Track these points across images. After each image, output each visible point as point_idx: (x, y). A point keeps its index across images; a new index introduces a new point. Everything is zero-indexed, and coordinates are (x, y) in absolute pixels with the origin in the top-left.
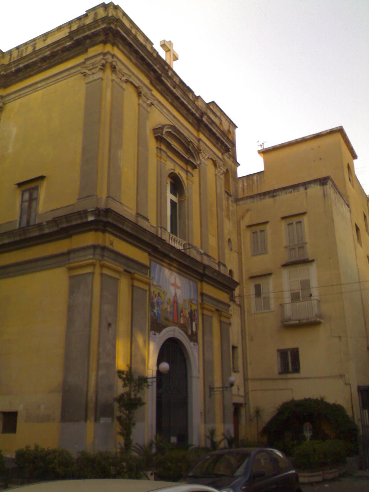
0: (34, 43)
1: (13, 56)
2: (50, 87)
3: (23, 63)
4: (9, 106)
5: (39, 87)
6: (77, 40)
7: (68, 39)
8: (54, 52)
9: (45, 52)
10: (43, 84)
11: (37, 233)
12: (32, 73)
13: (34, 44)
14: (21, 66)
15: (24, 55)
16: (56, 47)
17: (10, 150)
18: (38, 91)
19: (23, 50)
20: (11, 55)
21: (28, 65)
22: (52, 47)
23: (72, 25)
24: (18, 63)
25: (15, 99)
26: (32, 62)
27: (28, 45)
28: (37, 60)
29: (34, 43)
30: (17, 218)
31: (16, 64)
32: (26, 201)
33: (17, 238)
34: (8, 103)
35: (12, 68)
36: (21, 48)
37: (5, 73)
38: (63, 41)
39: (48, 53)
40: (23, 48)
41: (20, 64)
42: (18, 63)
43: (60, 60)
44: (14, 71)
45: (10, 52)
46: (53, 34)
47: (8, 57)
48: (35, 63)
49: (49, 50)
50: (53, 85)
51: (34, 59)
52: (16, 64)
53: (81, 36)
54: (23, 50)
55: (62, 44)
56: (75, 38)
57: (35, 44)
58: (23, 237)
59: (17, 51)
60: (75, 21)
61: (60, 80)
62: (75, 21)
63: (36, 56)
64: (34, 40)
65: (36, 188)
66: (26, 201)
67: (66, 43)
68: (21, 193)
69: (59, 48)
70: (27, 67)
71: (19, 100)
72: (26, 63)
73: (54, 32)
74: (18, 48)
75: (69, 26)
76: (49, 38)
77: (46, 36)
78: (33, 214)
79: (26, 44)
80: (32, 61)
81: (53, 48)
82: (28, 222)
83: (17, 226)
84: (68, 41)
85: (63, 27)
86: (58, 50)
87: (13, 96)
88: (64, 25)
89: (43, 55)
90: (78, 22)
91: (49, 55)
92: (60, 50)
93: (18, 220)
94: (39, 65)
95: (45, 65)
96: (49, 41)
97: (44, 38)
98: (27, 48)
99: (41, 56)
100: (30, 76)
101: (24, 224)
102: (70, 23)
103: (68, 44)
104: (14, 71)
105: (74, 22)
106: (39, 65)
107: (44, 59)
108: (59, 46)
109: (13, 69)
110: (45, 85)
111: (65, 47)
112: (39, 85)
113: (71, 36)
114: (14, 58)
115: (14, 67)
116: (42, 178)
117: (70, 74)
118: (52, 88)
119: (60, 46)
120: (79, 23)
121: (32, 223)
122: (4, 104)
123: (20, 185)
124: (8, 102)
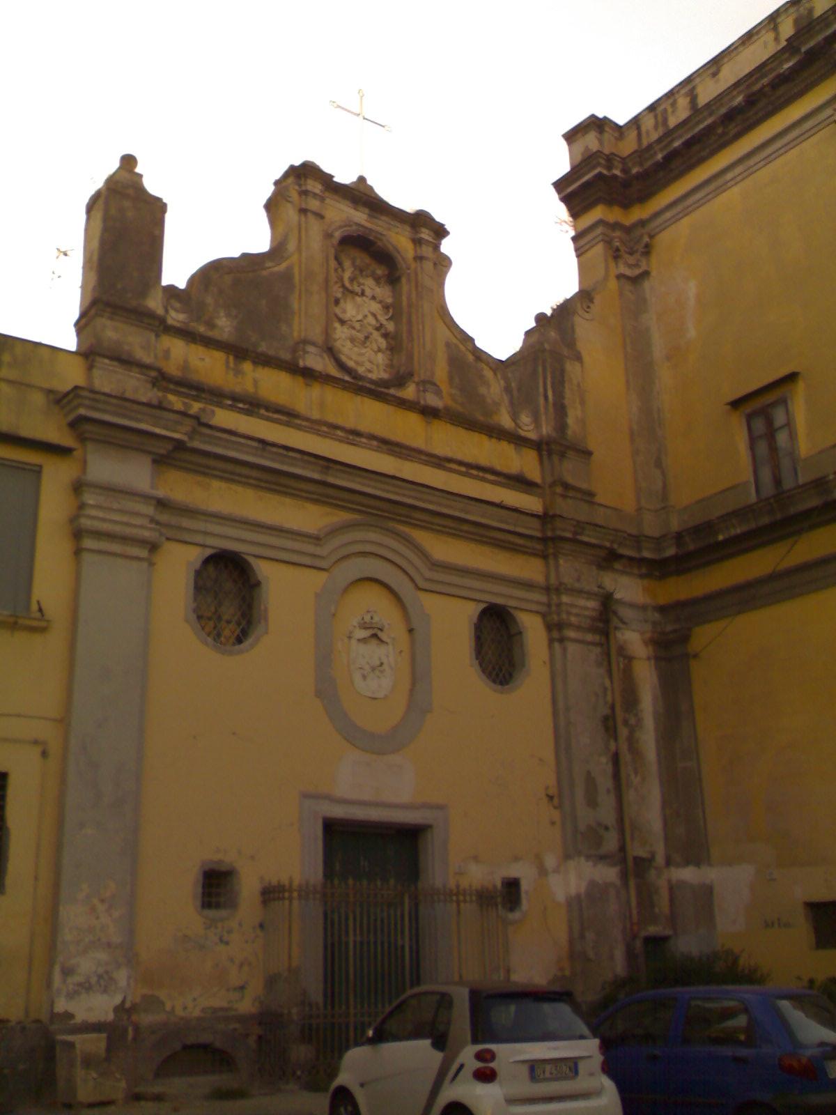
0: (689, 87)
1: (644, 129)
2: (758, 173)
3: (680, 136)
4: (664, 239)
5: (732, 179)
6: (807, 53)
7: (787, 55)
8: (754, 94)
9: (734, 98)
10: (738, 170)
11: (814, 502)
12: (703, 154)
13: (689, 91)
14: (677, 144)
15: (672, 122)
16: (757, 80)
17: (692, 333)
18: (730, 188)
19: (665, 110)
20: (638, 128)
21: (693, 137)
22: (747, 83)
23: (779, 20)
24: (669, 139)
25: (676, 219)
26: (704, 129)
27: (677, 96)
28: (714, 123)
29: (689, 87)
30: (748, 475)
31: (664, 144)
32: (781, 428)
33: (765, 520)
34: (660, 232)
35: (656, 153)
36: (660, 105)
37: (641, 170)
38: (772, 62)
39: (739, 99)
40: (666, 105)
41: (672, 141)
42: (669, 139)
43: (770, 108)
44: (661, 161)
45: (636, 122)
46: (733, 55)
47: (633, 135)
48: (710, 129)
49: (739, 93)
50: (764, 169)
51: (709, 121)
52: (664, 144)
53: (820, 37)
54: (665, 110)
55: (772, 70)
56: (803, 50)
57: (694, 88)
58: (779, 516)
59: (651, 115)
60: (786, 10)
61: (782, 151)
62: (786, 10)
63: (710, 115)
64: (689, 80)
65: (783, 402)
66: (781, 428)
67: (781, 64)
68: (744, 421)
69: (765, 81)
70: (688, 144)
71: (685, 221)
72: (688, 136)
73: (736, 48)
74: (652, 108)
75: (772, 26)
76: (725, 65)
77: (716, 63)
78: (785, 463)
79: (671, 94)
80: (702, 126)
81: (748, 87)
82: (777, 481)
83: (753, 498)
84: (787, 60)
85: (758, 33)
86: (764, 87)
87: (668, 215)
88: (760, 27)
89: (728, 106)
90: (792, 10)
91: (743, 104)
92: (768, 85)
93: (752, 480)
94: (720, 131)
95: (733, 129)
96: (729, 76)
97: (714, 69)
98: (674, 104)
99: (723, 111)
100: (702, 160)
101: (768, 489)
102: (773, 20)
103: (786, 66)
104: (661, 161)
105: (782, 13)
106: (720, 131)
107: (729, 117)
108: (762, 77)
109: (660, 156)
110: (744, 172)
111: (783, 74)
112: (729, 176)
113: (795, 44)
114: (648, 133)
115: (661, 150)
116: (792, 377)
117: (804, 133)
118: (764, 174)
119: (766, 76)
120: (798, 10)
121: (788, 484)
122: (652, 237)
123: (736, 404)
124: (657, 230)
